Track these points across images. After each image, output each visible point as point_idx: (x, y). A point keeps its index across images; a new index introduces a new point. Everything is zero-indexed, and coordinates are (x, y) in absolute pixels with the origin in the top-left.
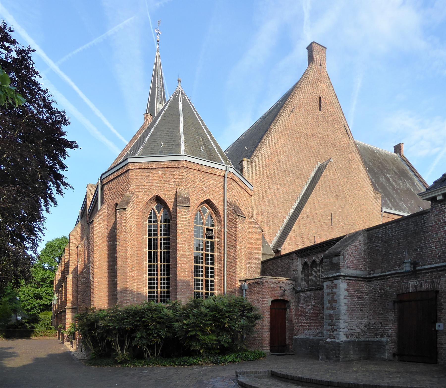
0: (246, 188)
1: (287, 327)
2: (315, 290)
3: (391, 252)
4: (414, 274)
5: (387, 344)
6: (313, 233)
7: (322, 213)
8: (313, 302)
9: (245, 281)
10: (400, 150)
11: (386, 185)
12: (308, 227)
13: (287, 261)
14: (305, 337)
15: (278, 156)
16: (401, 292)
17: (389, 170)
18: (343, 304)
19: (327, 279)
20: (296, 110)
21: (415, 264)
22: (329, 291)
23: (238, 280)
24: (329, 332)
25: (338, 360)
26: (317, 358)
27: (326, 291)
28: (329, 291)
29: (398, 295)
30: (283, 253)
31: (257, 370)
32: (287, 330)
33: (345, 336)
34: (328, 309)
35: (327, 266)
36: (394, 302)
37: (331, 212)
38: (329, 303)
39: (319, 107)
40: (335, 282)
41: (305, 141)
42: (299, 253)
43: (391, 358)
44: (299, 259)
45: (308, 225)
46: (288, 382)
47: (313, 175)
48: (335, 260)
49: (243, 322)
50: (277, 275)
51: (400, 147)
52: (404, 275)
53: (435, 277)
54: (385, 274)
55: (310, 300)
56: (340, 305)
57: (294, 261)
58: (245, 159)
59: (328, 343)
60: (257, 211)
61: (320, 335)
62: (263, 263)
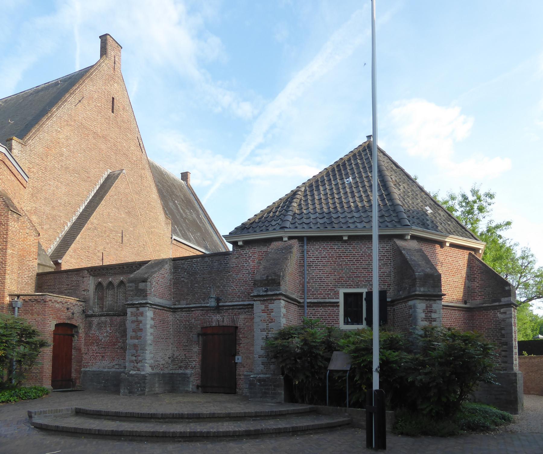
0: (20, 177)
1: (73, 357)
2: (112, 316)
3: (196, 285)
4: (218, 309)
5: (191, 376)
6: (101, 248)
7: (112, 228)
8: (108, 329)
9: (18, 296)
10: (187, 178)
11: (175, 211)
12: (96, 241)
13: (74, 278)
14: (97, 370)
15: (60, 147)
16: (205, 325)
17: (177, 196)
18: (149, 334)
19: (133, 305)
20: (85, 101)
21: (218, 300)
22: (134, 318)
23: (6, 294)
24: (132, 364)
25: (144, 394)
26: (117, 392)
27: (130, 317)
28: (134, 318)
29: (202, 328)
30: (64, 267)
31: (58, 409)
32: (73, 361)
33: (150, 368)
34: (132, 338)
35: (132, 291)
36: (199, 335)
37: (122, 228)
38: (134, 332)
39: (111, 108)
40: (141, 309)
41: (94, 141)
42: (91, 271)
43: (195, 390)
44: (91, 277)
45: (95, 239)
46: (102, 419)
47: (102, 182)
48: (141, 286)
49: (21, 349)
50: (61, 293)
51: (187, 176)
52: (207, 309)
53: (235, 314)
54: (190, 306)
55: (105, 327)
56: (146, 335)
57: (85, 279)
58: (15, 138)
59: (132, 375)
60: (29, 208)
61: (117, 367)
62: (38, 275)
